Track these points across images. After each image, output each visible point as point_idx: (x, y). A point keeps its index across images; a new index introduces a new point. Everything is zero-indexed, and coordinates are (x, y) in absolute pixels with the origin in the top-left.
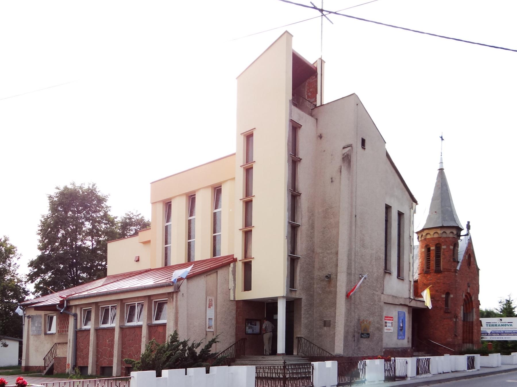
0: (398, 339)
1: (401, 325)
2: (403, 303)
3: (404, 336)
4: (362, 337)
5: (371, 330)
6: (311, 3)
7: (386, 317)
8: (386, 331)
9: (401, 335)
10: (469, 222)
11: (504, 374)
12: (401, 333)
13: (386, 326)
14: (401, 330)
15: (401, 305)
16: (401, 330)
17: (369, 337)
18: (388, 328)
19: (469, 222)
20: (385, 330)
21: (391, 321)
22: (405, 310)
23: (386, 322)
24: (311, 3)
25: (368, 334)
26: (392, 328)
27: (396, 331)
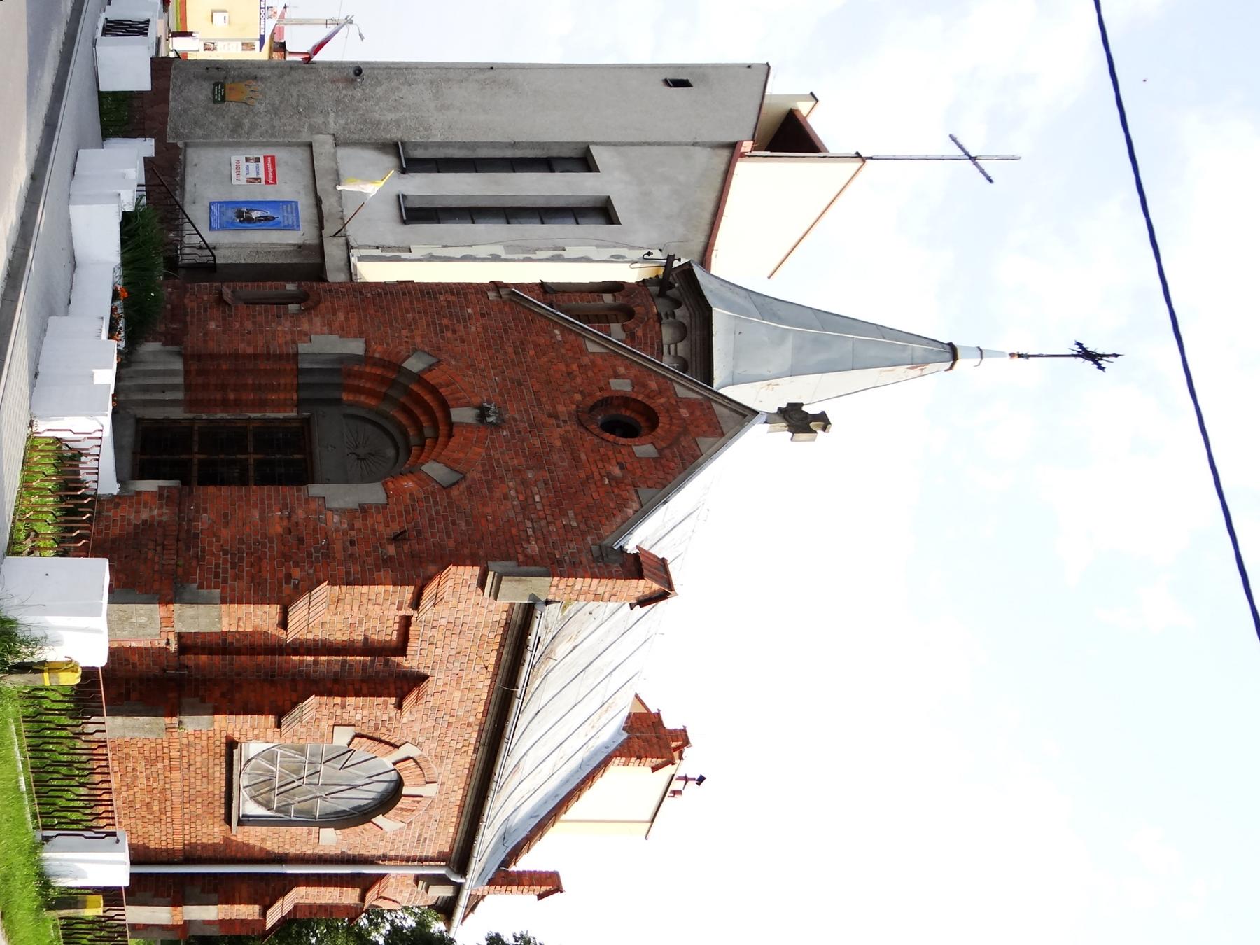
0: (212, 203)
1: (255, 215)
2: (325, 208)
3: (223, 228)
4: (216, 84)
5: (233, 108)
6: (1103, 369)
7: (273, 158)
8: (234, 159)
9: (222, 213)
10: (951, 136)
11: (42, 217)
12: (231, 213)
13: (247, 160)
14: (240, 214)
15: (318, 202)
16: (240, 214)
17: (215, 101)
18: (243, 165)
19: (951, 136)
20: (237, 157)
21: (262, 175)
22: (303, 235)
23: (257, 160)
24: (1103, 369)
25: (223, 99)
26: (243, 180)
27: (241, 196)
